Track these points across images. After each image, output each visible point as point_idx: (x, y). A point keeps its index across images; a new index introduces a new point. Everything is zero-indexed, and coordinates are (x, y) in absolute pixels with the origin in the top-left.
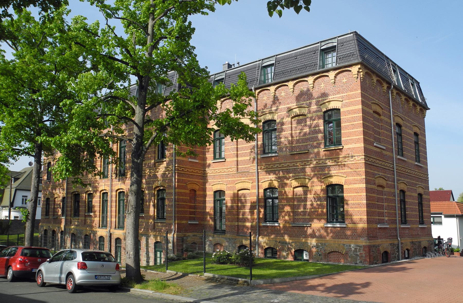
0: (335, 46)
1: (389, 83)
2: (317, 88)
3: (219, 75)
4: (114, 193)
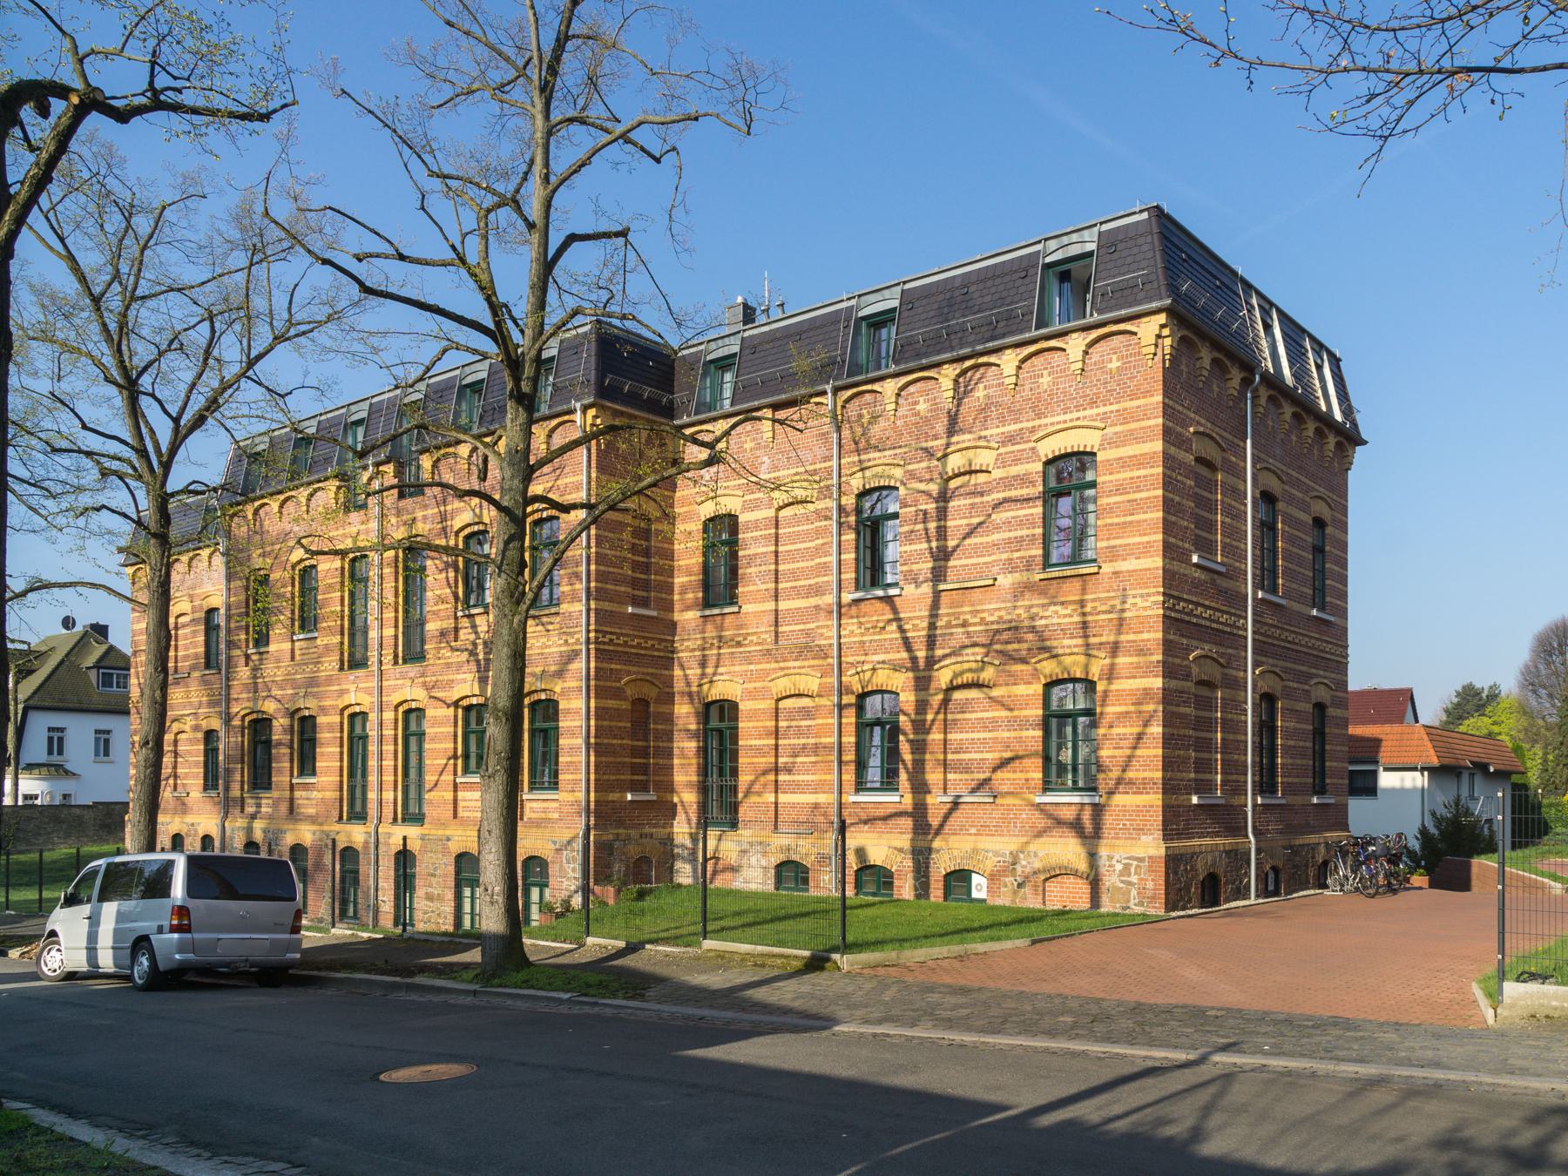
0: (1091, 254)
1: (1249, 366)
2: (1027, 387)
3: (720, 343)
4: (389, 715)
